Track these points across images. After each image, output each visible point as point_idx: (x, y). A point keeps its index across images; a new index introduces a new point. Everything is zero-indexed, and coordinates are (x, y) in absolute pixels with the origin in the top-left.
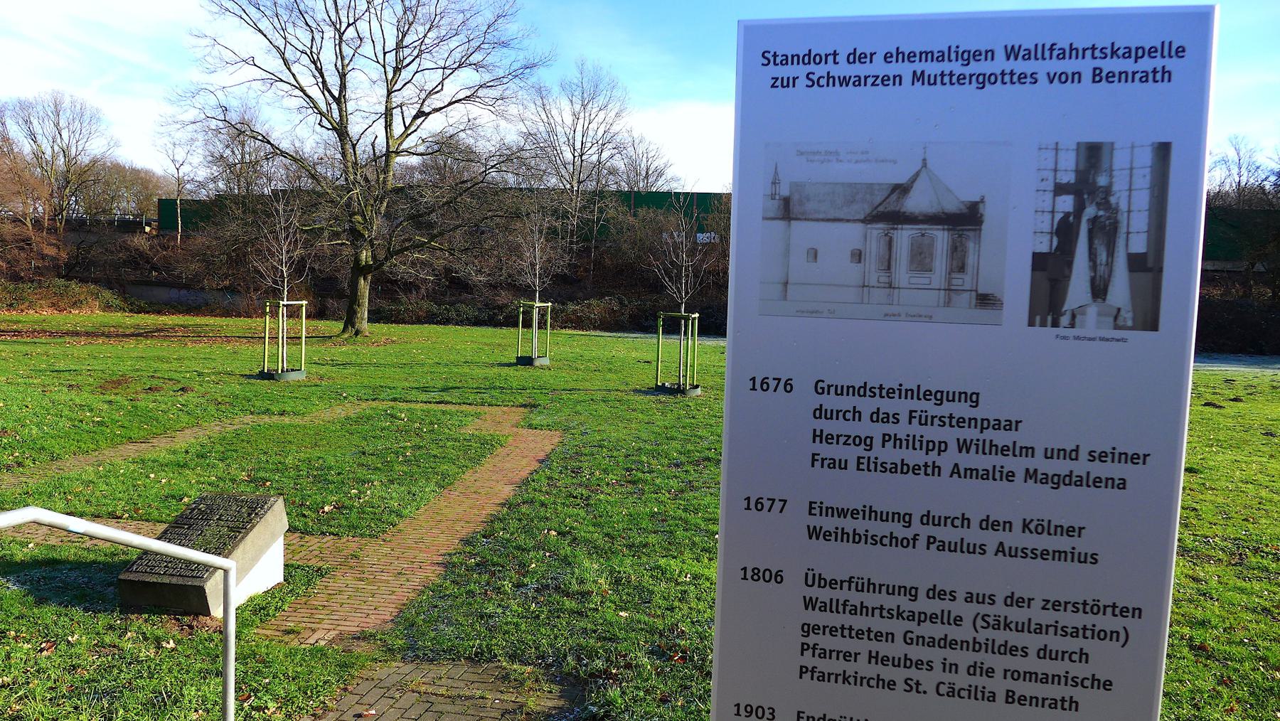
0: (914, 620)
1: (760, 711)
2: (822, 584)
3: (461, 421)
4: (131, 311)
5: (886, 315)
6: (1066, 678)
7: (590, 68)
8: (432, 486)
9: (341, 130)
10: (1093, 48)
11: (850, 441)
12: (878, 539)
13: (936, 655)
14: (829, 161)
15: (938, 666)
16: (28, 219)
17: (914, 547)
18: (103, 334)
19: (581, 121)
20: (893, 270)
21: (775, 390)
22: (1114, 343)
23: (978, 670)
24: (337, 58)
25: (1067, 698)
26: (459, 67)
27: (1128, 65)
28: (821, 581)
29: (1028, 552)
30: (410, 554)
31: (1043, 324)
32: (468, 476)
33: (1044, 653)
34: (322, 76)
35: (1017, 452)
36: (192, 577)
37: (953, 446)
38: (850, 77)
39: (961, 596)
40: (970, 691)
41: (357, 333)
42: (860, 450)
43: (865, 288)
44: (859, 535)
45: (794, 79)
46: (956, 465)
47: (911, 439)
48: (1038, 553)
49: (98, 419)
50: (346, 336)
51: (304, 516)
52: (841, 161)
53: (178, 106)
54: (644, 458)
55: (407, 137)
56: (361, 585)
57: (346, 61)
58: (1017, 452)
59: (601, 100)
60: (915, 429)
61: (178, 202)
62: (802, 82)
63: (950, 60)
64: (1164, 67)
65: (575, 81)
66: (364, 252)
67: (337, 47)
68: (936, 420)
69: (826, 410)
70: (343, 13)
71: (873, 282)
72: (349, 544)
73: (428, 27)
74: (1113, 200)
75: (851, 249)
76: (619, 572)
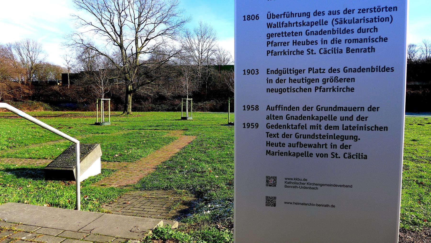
0: (318, 120)
4: (54, 110)
7: (204, 24)
8: (152, 149)
9: (121, 46)
13: (318, 38)
16: (19, 82)
18: (44, 116)
19: (201, 42)
23: (335, 41)
24: (119, 22)
25: (370, 47)
26: (160, 23)
28: (273, 16)
30: (144, 166)
32: (164, 147)
33: (360, 30)
34: (114, 27)
36: (69, 167)
39: (326, 13)
41: (128, 113)
49: (41, 135)
50: (124, 114)
51: (109, 157)
53: (67, 39)
54: (224, 141)
55: (143, 48)
56: (127, 174)
57: (122, 23)
59: (207, 35)
61: (68, 74)
65: (199, 29)
66: (130, 86)
67: (119, 18)
70: (120, 6)
72: (123, 164)
73: (149, 10)
76: (215, 167)
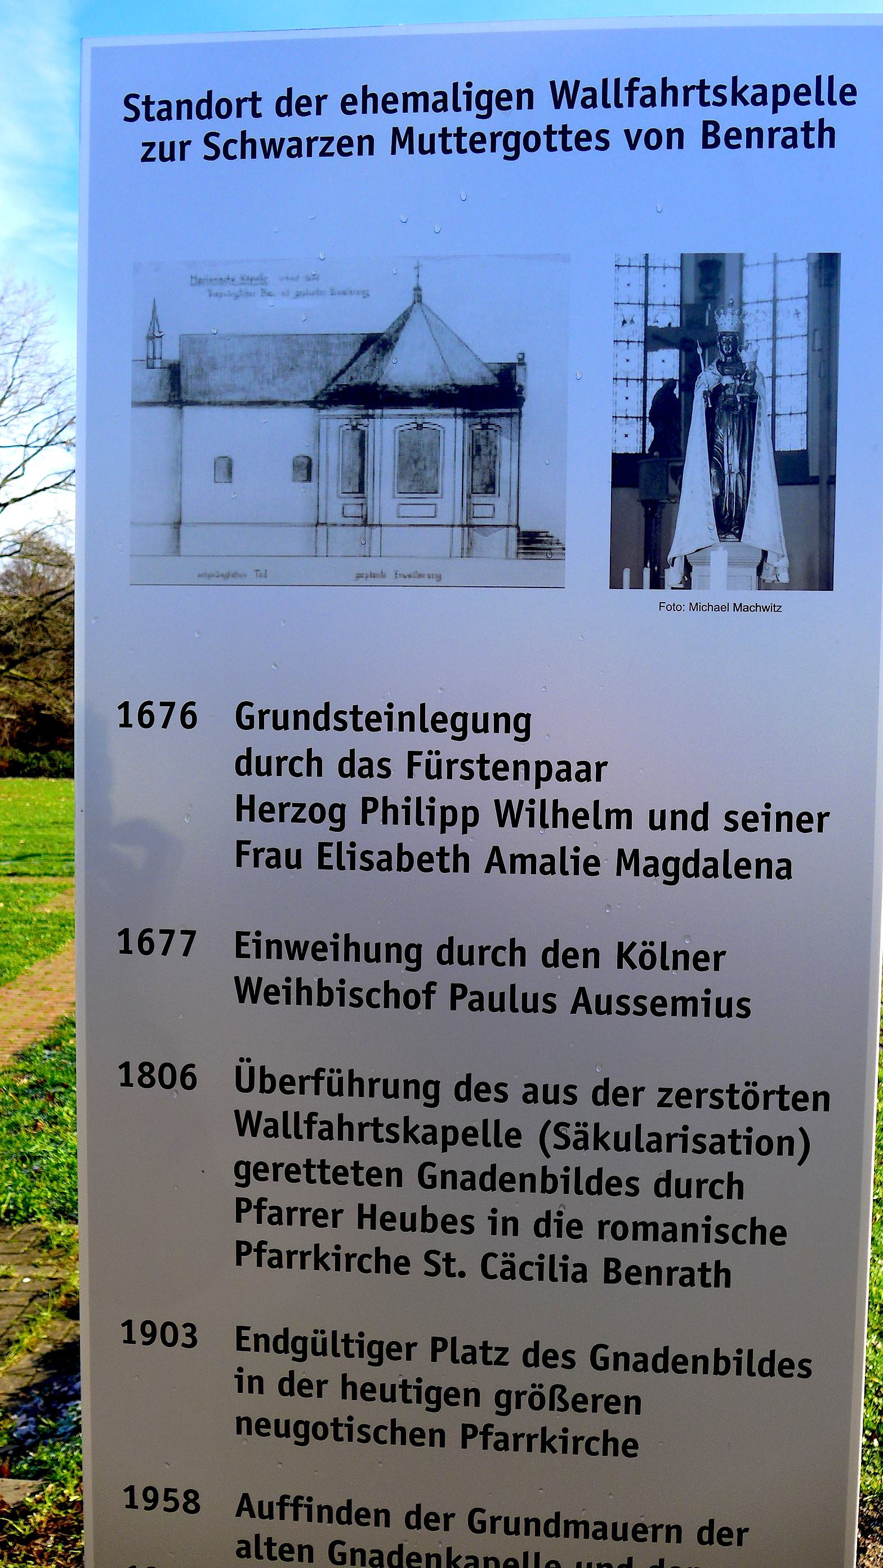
1: (169, 1331)
2: (268, 1085)
3: (38, 897)
5: (359, 576)
6: (707, 1227)
10: (702, 87)
11: (305, 814)
12: (363, 995)
14: (249, 294)
15: (481, 1224)
17: (428, 1006)
20: (368, 491)
21: (165, 726)
22: (760, 614)
23: (554, 1226)
26: (47, 444)
27: (762, 117)
29: (630, 1002)
31: (637, 584)
32: (37, 969)
35: (602, 820)
37: (488, 816)
38: (282, 140)
39: (515, 1091)
40: (541, 1266)
42: (323, 831)
43: (320, 528)
44: (329, 989)
45: (183, 145)
46: (496, 850)
47: (413, 805)
48: (647, 1003)
52: (269, 295)
58: (602, 820)
60: (421, 786)
62: (198, 150)
63: (457, 109)
64: (821, 121)
68: (457, 769)
69: (258, 759)
71: (335, 517)
74: (745, 356)
75: (291, 457)
